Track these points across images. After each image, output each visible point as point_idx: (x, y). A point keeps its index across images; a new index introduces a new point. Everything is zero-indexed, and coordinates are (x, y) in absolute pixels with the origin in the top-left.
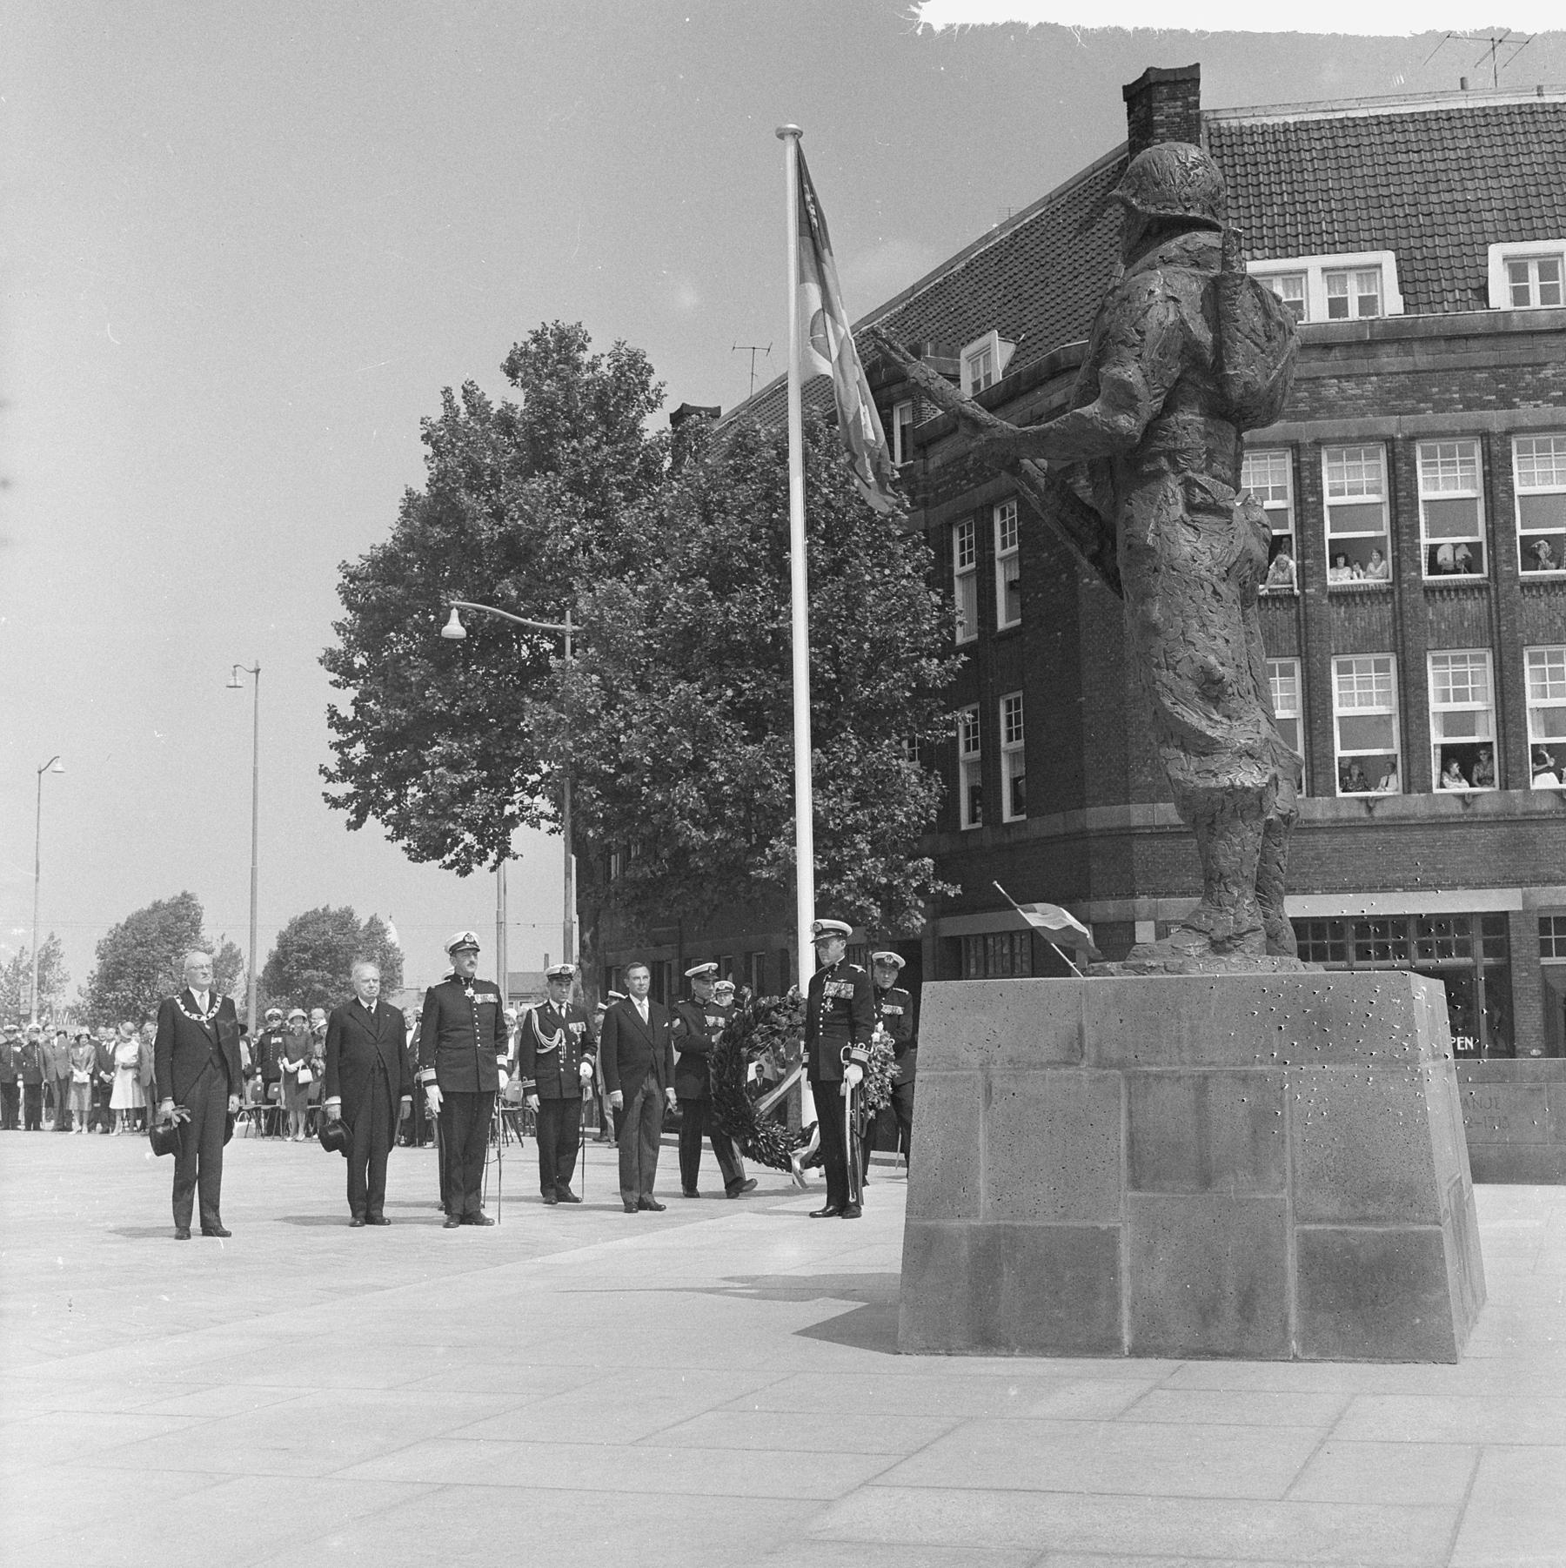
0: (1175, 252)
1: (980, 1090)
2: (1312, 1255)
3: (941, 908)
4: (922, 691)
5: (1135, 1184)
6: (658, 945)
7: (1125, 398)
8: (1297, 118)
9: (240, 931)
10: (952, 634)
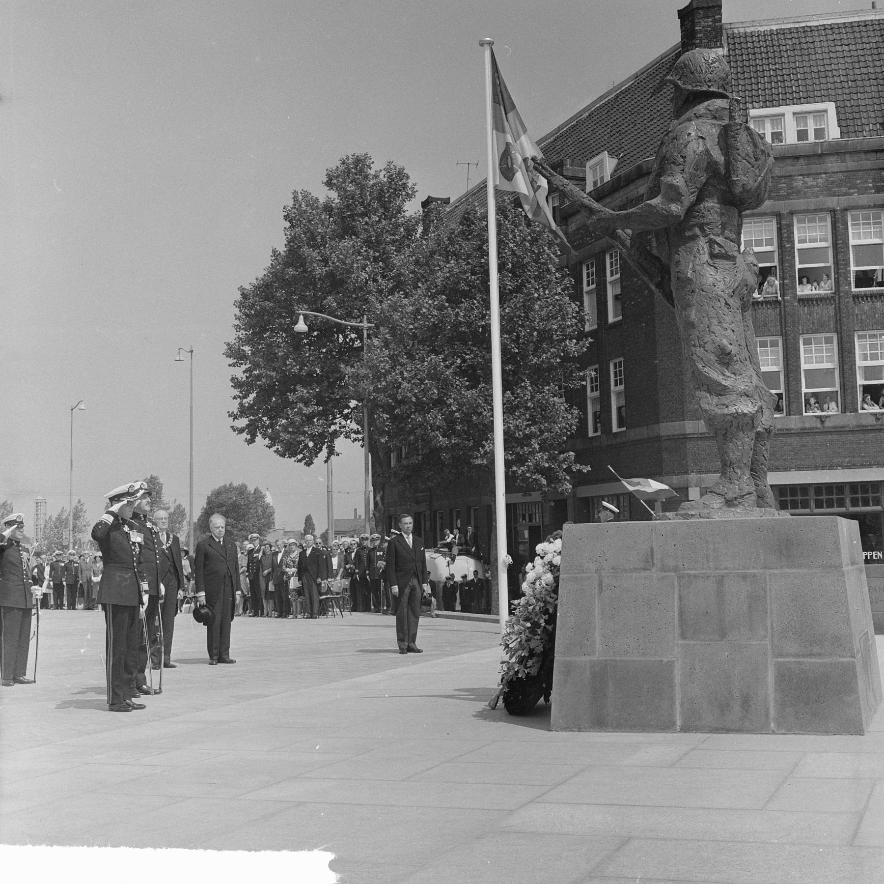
0: (703, 111)
1: (596, 583)
2: (784, 677)
3: (579, 480)
4: (566, 358)
5: (683, 636)
6: (418, 503)
7: (675, 194)
8: (778, 27)
9: (185, 498)
10: (583, 326)
